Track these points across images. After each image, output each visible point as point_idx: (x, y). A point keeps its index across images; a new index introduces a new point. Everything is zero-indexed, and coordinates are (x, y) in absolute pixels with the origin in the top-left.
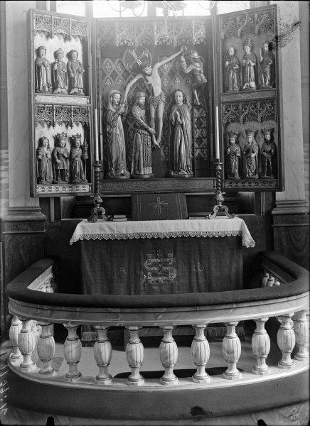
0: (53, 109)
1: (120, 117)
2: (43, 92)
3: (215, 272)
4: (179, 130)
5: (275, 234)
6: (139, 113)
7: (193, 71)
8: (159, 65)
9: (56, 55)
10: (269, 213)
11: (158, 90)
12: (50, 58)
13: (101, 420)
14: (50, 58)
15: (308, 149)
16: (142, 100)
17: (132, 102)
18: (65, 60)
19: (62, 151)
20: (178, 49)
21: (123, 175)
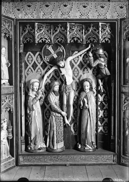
4: (86, 111)
8: (70, 59)
11: (69, 80)
16: (56, 88)
21: (39, 149)
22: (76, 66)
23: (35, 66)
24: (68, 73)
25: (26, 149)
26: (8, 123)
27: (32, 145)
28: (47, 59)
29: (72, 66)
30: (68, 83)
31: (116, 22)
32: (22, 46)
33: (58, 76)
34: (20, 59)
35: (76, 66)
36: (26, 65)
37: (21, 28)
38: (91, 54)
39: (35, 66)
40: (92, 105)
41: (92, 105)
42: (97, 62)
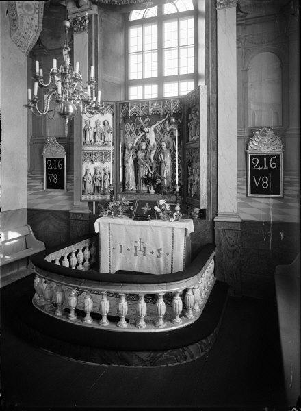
0: (92, 153)
1: (131, 157)
2: (88, 145)
3: (88, 7)
4: (163, 165)
5: (216, 233)
6: (141, 155)
7: (172, 129)
8: (154, 126)
9: (96, 123)
10: (214, 222)
11: (153, 141)
12: (93, 125)
13: (102, 253)
14: (93, 125)
15: (297, 312)
16: (144, 147)
17: (138, 148)
18: (102, 125)
19: (98, 176)
20: (165, 116)
21: (131, 190)
22: (158, 131)
23: (131, 132)
24: (152, 138)
25: (123, 191)
26: (115, 162)
27: (127, 188)
28: (138, 127)
29: (155, 131)
30: (152, 144)
31: (279, 194)
32: (122, 119)
33: (145, 139)
34: (120, 128)
35: (158, 131)
36: (125, 132)
37: (16, 241)
38: (167, 122)
39: (131, 132)
40: (167, 161)
41: (167, 161)
42: (171, 127)
